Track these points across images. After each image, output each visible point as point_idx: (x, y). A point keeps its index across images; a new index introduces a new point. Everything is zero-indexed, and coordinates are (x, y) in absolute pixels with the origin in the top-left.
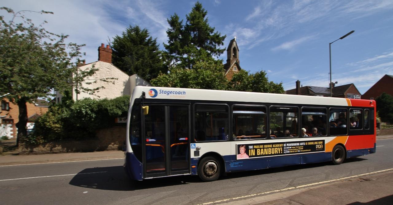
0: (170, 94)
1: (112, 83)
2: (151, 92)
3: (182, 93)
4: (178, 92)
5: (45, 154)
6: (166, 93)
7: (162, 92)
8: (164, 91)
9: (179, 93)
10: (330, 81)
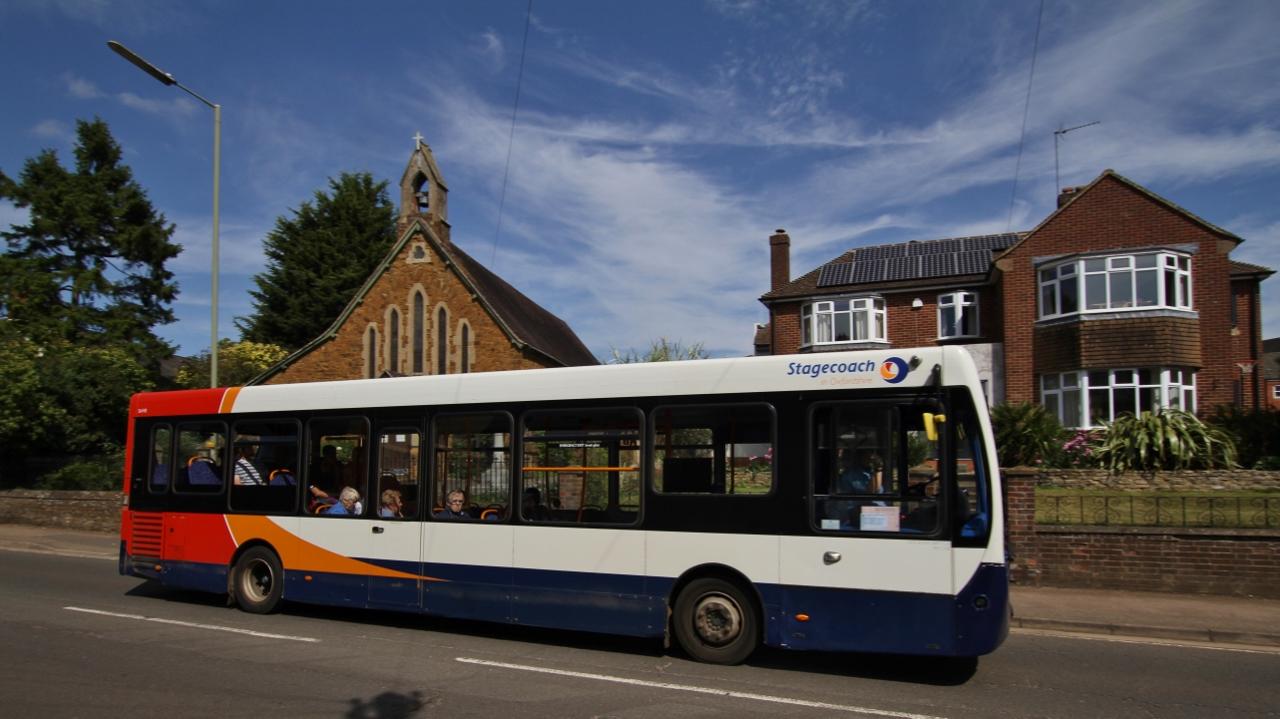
0: (821, 372)
1: (405, 365)
2: (888, 366)
3: (863, 367)
4: (847, 371)
5: (1088, 587)
6: (808, 372)
7: (796, 369)
8: (803, 365)
9: (852, 368)
10: (766, 272)
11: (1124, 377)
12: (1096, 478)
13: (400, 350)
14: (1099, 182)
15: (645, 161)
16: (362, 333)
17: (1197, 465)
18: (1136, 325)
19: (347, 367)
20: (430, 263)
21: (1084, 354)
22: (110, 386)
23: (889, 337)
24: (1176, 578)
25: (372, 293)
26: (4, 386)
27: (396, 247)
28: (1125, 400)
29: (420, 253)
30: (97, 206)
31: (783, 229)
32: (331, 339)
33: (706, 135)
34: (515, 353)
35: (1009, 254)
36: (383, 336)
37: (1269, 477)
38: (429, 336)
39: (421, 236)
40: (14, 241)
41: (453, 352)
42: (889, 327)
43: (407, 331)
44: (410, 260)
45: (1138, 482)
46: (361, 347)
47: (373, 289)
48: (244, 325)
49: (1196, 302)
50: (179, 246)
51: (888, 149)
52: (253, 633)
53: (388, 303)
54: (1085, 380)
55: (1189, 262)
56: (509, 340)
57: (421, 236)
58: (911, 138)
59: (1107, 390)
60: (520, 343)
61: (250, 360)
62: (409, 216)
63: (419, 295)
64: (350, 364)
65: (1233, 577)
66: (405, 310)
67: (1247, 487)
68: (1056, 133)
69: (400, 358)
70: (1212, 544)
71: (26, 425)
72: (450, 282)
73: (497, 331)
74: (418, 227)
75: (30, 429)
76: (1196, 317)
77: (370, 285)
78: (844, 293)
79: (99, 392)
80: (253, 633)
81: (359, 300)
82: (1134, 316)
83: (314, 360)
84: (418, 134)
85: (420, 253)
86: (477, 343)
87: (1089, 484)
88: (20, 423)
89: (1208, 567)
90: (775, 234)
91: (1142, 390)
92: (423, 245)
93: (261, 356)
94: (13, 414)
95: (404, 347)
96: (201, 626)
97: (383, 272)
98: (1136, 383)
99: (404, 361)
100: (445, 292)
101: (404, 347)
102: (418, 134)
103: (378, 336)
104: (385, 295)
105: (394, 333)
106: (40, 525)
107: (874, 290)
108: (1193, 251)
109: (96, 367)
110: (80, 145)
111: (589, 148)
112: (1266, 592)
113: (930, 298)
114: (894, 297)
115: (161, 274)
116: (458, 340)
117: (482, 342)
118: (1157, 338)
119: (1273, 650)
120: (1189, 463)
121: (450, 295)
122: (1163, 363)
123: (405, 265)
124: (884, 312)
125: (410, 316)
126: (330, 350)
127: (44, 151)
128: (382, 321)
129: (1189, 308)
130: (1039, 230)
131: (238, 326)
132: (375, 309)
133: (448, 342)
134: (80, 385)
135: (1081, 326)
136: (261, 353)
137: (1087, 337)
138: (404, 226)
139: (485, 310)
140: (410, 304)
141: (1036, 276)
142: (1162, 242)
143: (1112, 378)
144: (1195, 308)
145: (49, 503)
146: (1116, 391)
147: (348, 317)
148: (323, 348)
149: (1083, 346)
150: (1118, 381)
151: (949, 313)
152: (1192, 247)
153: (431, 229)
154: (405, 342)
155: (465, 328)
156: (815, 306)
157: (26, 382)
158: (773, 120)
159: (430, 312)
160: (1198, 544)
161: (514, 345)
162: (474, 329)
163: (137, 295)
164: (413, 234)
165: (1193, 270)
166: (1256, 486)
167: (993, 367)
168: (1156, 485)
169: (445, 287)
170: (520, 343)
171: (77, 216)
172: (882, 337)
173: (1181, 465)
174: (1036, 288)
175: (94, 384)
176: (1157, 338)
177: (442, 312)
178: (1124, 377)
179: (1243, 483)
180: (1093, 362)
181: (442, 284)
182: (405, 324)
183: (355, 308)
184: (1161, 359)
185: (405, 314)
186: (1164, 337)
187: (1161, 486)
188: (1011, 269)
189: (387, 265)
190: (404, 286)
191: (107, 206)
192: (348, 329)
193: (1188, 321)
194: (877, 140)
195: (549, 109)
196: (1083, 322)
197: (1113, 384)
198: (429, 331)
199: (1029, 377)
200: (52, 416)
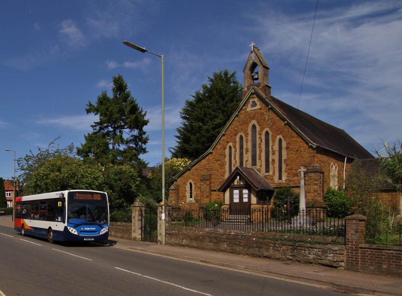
16: (225, 149)
20: (260, 109)
25: (230, 129)
27: (242, 104)
29: (254, 104)
32: (210, 153)
34: (312, 151)
38: (260, 147)
41: (273, 154)
44: (249, 108)
60: (315, 145)
61: (176, 166)
63: (254, 126)
64: (220, 165)
73: (299, 140)
74: (253, 91)
81: (223, 133)
83: (203, 164)
84: (252, 43)
86: (287, 148)
92: (256, 100)
93: (180, 164)
95: (246, 153)
101: (246, 153)
103: (233, 149)
105: (241, 147)
115: (142, 133)
116: (276, 147)
121: (271, 124)
123: (247, 112)
125: (250, 138)
128: (235, 142)
131: (170, 151)
134: (116, 181)
136: (180, 162)
139: (292, 129)
140: (250, 131)
154: (247, 151)
155: (280, 140)
175: (120, 180)
177: (267, 133)
181: (267, 118)
192: (219, 148)
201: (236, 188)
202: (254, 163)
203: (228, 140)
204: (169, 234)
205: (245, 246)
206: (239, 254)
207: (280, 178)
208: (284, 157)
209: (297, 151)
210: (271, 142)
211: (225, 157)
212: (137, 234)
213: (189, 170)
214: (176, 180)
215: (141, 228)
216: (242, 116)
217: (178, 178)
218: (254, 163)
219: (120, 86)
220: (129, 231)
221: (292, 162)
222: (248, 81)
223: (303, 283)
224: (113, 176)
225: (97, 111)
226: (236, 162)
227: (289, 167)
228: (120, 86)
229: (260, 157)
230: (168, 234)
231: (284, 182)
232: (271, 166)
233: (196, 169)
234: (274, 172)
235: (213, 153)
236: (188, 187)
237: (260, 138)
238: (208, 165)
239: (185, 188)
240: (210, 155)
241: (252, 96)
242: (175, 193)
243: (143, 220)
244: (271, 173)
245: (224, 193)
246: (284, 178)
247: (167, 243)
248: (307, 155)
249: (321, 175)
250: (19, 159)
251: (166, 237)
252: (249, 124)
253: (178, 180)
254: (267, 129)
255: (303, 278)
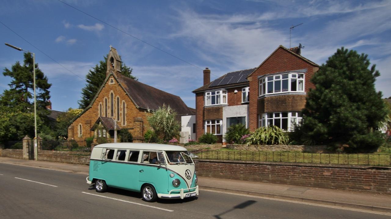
11: (277, 115)
12: (244, 147)
13: (108, 110)
14: (278, 50)
15: (257, 28)
16: (98, 105)
17: (269, 143)
18: (281, 98)
19: (95, 115)
20: (115, 84)
21: (265, 108)
22: (28, 123)
23: (228, 103)
24: (199, 172)
25: (100, 94)
26: (1, 124)
27: (106, 80)
28: (277, 122)
29: (112, 81)
30: (26, 75)
31: (208, 68)
32: (91, 107)
33: (282, 15)
34: (137, 110)
35: (251, 75)
36: (103, 106)
37: (287, 147)
38: (115, 106)
39: (112, 76)
40: (11, 86)
41: (121, 110)
42: (228, 99)
43: (109, 104)
44: (110, 83)
45: (254, 148)
46: (98, 109)
47: (100, 93)
48: (80, 103)
49: (306, 89)
50: (51, 84)
51: (364, 12)
52: (114, 199)
53: (104, 96)
54: (266, 116)
55: (304, 75)
56: (135, 106)
57: (112, 76)
58: (376, 5)
59: (272, 119)
60: (138, 107)
61: (75, 114)
62: (109, 70)
63: (112, 94)
64: (95, 115)
65: (209, 172)
66: (109, 98)
67: (281, 150)
68: (291, 28)
69: (108, 112)
70: (205, 163)
71: (7, 133)
72: (120, 89)
73: (132, 104)
74: (111, 74)
75: (8, 134)
76: (305, 94)
77: (99, 91)
78: (214, 89)
79: (26, 125)
80: (114, 199)
81: (97, 96)
82: (280, 95)
83: (87, 114)
84: (111, 45)
85: (112, 81)
86: (127, 107)
87: (242, 149)
88: (5, 133)
89: (204, 169)
90: (205, 69)
91: (282, 119)
92: (113, 79)
93: (78, 113)
94: (3, 131)
95: (108, 109)
96: (119, 200)
97: (103, 87)
98: (281, 117)
99: (109, 113)
100: (119, 92)
101: (108, 109)
102: (111, 45)
103: (102, 106)
104: (104, 94)
105: (106, 105)
106: (10, 157)
107: (223, 88)
108: (305, 72)
109: (25, 119)
110: (25, 59)
111: (235, 26)
112: (381, 190)
113: (240, 89)
114: (230, 90)
115: (48, 93)
116: (122, 107)
117: (128, 107)
118: (287, 102)
119: (388, 214)
120: (266, 143)
121: (120, 93)
122: (288, 110)
123: (109, 85)
124: (226, 95)
125: (110, 100)
126: (91, 111)
127: (17, 62)
128: (103, 102)
129: (303, 91)
130: (260, 67)
131: (79, 103)
132: (101, 99)
133: (119, 107)
134: (21, 123)
135: (265, 99)
136: (78, 112)
137: (267, 102)
138: (108, 73)
139: (129, 98)
140: (110, 96)
141: (258, 82)
142: (290, 70)
143: (274, 115)
144: (305, 91)
145: (11, 152)
146: (275, 120)
147: (95, 101)
148: (89, 110)
149: (265, 105)
150: (276, 116)
151: (244, 94)
152: (304, 70)
153: (115, 74)
154: (109, 108)
155: (124, 103)
156: (206, 93)
157: (6, 123)
158: (311, 6)
159: (115, 99)
160: (203, 163)
161: (136, 108)
162: (126, 103)
163: (42, 98)
164: (110, 76)
165: (305, 78)
166: (283, 150)
167: (248, 112)
168: (258, 149)
169: (119, 91)
170: (138, 107)
171: (23, 79)
172: (226, 103)
173: (264, 143)
174: (259, 85)
175: (25, 123)
176: (287, 102)
177: (118, 98)
178: (277, 115)
179: (280, 149)
180: (268, 110)
181: (118, 90)
182: (109, 103)
183: (96, 98)
184: (288, 109)
185: (109, 99)
186: (289, 102)
187: (259, 150)
188: (252, 80)
189: (104, 85)
190: (108, 91)
191: (30, 75)
192: (95, 105)
193: (300, 96)
194: (359, 8)
195: (220, 13)
196: (266, 97)
197: (274, 117)
198: (115, 104)
199: (255, 115)
200: (12, 131)
201: (99, 129)
202: (112, 115)
203: (100, 101)
204: (39, 155)
205: (66, 159)
206: (63, 163)
207: (124, 124)
208: (126, 112)
209: (131, 109)
210: (120, 103)
211: (98, 110)
212: (26, 155)
213: (79, 117)
214: (72, 123)
215: (29, 152)
216: (106, 87)
217: (73, 122)
218: (112, 115)
219: (29, 59)
220: (21, 154)
221: (129, 115)
222: (109, 67)
223: (231, 193)
224: (19, 120)
225: (11, 74)
226: (103, 113)
227: (128, 118)
228: (29, 59)
229: (115, 111)
230: (39, 155)
231: (126, 126)
232: (120, 117)
233: (83, 117)
234: (121, 120)
235: (92, 108)
236: (79, 127)
237: (115, 101)
238: (90, 115)
239: (77, 128)
240: (90, 108)
241: (111, 76)
242: (71, 131)
243: (30, 148)
244: (120, 121)
245: (94, 132)
246: (126, 124)
247: (38, 160)
248: (136, 112)
249: (142, 123)
250: (119, 62)
251: (38, 156)
252: (109, 92)
253: (74, 123)
254: (118, 96)
255: (289, 197)
